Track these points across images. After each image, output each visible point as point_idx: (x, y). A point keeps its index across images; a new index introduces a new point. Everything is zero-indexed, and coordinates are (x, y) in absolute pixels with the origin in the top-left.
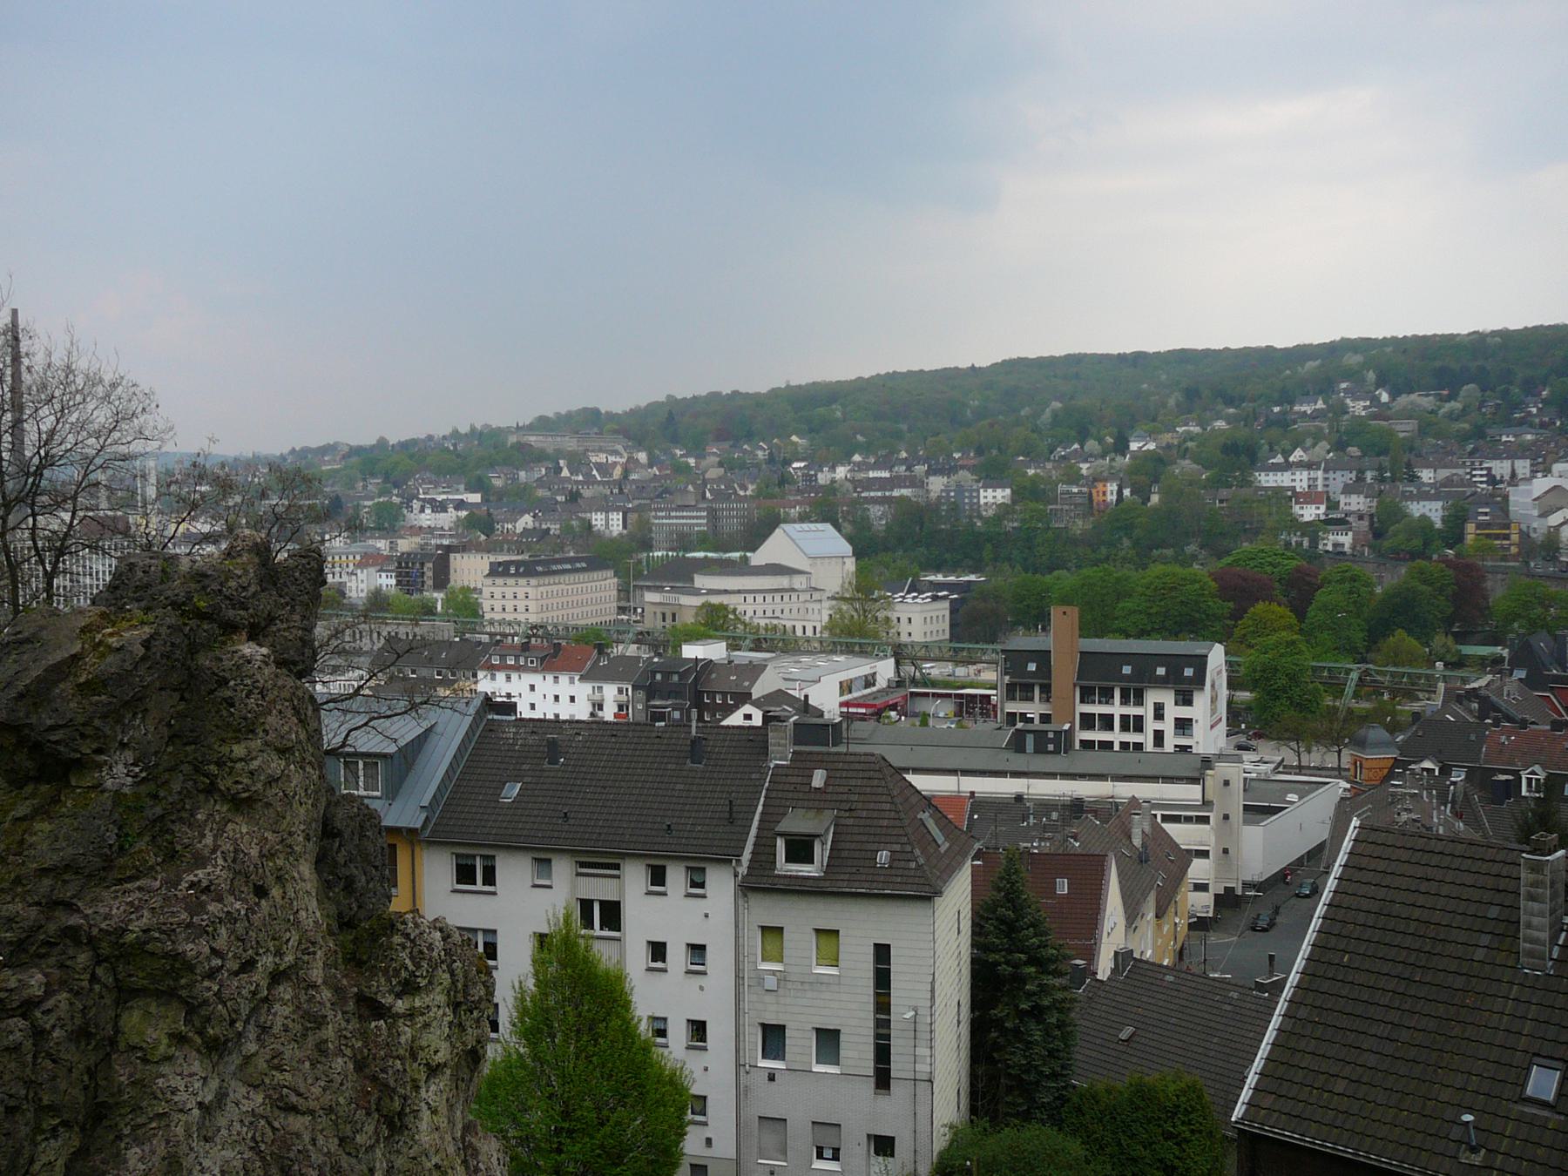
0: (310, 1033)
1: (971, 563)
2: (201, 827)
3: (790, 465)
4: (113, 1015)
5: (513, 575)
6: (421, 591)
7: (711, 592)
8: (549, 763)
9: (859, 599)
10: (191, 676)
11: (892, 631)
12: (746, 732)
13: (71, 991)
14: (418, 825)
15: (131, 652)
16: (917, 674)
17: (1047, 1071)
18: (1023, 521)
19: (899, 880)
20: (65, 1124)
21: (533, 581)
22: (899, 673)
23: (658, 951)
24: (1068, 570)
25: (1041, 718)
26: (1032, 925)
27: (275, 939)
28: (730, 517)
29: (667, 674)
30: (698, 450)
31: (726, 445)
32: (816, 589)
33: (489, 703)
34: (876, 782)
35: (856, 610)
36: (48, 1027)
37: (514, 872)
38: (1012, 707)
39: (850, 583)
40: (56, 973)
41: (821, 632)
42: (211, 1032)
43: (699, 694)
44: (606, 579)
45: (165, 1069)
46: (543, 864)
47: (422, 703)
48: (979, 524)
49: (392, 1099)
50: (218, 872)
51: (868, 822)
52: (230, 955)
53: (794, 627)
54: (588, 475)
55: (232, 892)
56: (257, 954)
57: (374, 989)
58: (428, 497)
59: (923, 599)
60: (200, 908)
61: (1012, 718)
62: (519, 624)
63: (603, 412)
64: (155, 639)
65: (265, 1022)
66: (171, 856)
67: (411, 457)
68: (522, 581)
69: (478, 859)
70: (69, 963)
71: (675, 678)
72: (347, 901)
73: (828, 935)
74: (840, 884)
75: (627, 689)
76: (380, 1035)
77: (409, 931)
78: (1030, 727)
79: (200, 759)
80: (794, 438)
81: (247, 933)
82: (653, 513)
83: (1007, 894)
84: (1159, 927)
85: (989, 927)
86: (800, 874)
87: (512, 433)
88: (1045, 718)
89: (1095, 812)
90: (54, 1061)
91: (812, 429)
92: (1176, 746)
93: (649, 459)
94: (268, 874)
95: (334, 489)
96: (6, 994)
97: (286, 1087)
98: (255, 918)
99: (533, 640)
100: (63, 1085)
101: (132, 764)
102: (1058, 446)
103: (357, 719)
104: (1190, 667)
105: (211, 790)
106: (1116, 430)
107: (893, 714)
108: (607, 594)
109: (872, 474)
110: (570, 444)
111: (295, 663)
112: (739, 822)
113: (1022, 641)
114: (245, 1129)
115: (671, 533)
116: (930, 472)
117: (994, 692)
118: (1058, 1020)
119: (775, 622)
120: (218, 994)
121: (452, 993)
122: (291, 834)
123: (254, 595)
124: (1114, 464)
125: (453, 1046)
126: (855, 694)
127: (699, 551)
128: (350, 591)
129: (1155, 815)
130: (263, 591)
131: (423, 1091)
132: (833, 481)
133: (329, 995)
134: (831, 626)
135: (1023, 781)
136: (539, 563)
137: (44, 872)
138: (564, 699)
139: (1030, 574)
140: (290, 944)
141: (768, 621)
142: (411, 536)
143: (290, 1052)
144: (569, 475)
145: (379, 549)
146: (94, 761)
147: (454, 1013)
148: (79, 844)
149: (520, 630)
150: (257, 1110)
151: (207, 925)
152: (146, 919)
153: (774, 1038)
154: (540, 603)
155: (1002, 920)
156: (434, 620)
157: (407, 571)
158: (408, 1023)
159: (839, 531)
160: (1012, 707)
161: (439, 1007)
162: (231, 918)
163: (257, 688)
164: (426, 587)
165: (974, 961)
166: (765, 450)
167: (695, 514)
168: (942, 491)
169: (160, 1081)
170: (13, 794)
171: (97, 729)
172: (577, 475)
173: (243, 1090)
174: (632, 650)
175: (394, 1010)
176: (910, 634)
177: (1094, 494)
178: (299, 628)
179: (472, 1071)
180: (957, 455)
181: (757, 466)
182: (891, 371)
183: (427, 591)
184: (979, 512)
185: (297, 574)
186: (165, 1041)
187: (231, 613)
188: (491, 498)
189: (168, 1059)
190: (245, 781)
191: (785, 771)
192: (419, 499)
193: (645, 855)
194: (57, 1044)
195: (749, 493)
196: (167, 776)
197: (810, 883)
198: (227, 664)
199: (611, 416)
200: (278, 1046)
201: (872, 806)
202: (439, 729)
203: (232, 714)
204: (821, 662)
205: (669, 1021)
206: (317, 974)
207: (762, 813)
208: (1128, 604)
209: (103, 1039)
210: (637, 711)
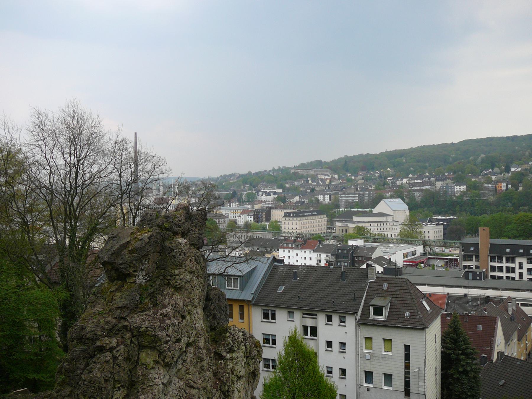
0: (199, 363)
1: (451, 212)
2: (165, 296)
3: (387, 179)
4: (138, 354)
5: (292, 217)
6: (262, 222)
7: (359, 222)
8: (294, 280)
9: (410, 225)
10: (163, 248)
11: (422, 236)
12: (315, 268)
13: (124, 345)
14: (251, 299)
15: (144, 241)
16: (431, 251)
17: (469, 394)
18: (471, 197)
19: (413, 322)
20: (122, 386)
21: (299, 219)
22: (424, 250)
23: (329, 344)
24: (488, 214)
25: (476, 267)
26: (463, 341)
27: (188, 332)
28: (366, 197)
29: (343, 251)
30: (355, 174)
31: (365, 172)
32: (395, 221)
33: (275, 260)
34: (405, 288)
35: (409, 228)
36: (117, 356)
37: (281, 315)
38: (465, 263)
39: (407, 219)
40: (120, 340)
41: (397, 236)
42: (166, 361)
43: (354, 257)
44: (323, 218)
45: (152, 371)
46: (291, 313)
47: (249, 259)
48: (454, 198)
49: (225, 386)
50: (169, 310)
51: (402, 302)
52: (173, 336)
53: (388, 234)
54: (318, 183)
55: (174, 317)
56: (181, 337)
57: (220, 350)
58: (264, 190)
59: (434, 225)
60: (164, 321)
61: (465, 266)
62: (294, 233)
63: (323, 161)
64: (152, 237)
65: (184, 359)
66: (156, 305)
67: (259, 177)
68: (295, 219)
69: (270, 311)
70: (124, 336)
71: (346, 252)
72: (214, 322)
73: (387, 341)
74: (392, 323)
75: (329, 255)
76: (222, 365)
77: (232, 332)
78: (471, 270)
79: (165, 274)
80: (388, 169)
81: (178, 330)
82: (340, 196)
83: (454, 329)
84: (519, 345)
85: (447, 340)
86: (378, 319)
87: (293, 169)
88: (477, 267)
89: (493, 302)
90: (119, 367)
91: (394, 166)
92: (528, 278)
93: (338, 177)
94: (185, 311)
95: (234, 188)
96: (106, 345)
97: (190, 380)
98: (181, 325)
99: (299, 238)
100: (122, 374)
101: (145, 276)
102: (484, 170)
103: (229, 264)
104: (472, 247)
105: (168, 284)
106: (505, 164)
107: (422, 265)
108: (324, 223)
109: (416, 181)
110: (312, 172)
111: (196, 245)
112: (357, 301)
113: (468, 240)
114: (177, 392)
115: (346, 202)
116: (436, 180)
117: (458, 258)
118: (473, 376)
119: (381, 232)
120: (168, 349)
121: (246, 353)
122: (193, 299)
123: (183, 223)
124: (505, 176)
125: (246, 371)
126: (409, 258)
127: (355, 208)
128: (239, 222)
129: (518, 303)
130: (187, 222)
131: (236, 384)
132: (402, 184)
133: (206, 351)
134: (401, 234)
135: (467, 290)
136: (301, 212)
137: (118, 308)
138: (308, 259)
139: (473, 216)
140: (193, 334)
141: (378, 232)
142: (259, 204)
143: (192, 369)
144: (311, 183)
145: (248, 208)
146: (133, 274)
147: (246, 359)
148: (128, 300)
149: (294, 235)
150: (181, 387)
151: (165, 327)
152: (147, 324)
153: (369, 375)
154: (301, 226)
155: (452, 339)
156: (265, 232)
157: (257, 215)
158: (231, 362)
159: (404, 201)
160: (465, 263)
161: (241, 357)
162: (173, 325)
163: (183, 252)
164: (263, 221)
165: (442, 353)
166: (378, 173)
167: (354, 196)
168: (441, 187)
169: (151, 375)
170: (111, 284)
171: (134, 264)
172: (314, 183)
173: (177, 380)
174: (332, 242)
175: (226, 357)
176: (429, 237)
177: (497, 187)
178: (198, 234)
179: (254, 379)
180: (446, 174)
181: (376, 179)
182: (423, 145)
183: (264, 222)
184: (454, 194)
185: (198, 216)
186: (152, 363)
187: (176, 229)
188: (285, 191)
189: (153, 368)
190: (179, 282)
191: (373, 284)
192: (261, 191)
193: (325, 311)
194: (120, 361)
195: (372, 188)
196: (155, 279)
197: (381, 323)
198: (174, 245)
199: (325, 163)
200: (189, 367)
201: (404, 296)
202: (258, 268)
203: (175, 260)
204: (397, 246)
205: (333, 368)
206: (201, 344)
207: (365, 298)
208: (510, 226)
209: (134, 361)
210: (329, 264)
